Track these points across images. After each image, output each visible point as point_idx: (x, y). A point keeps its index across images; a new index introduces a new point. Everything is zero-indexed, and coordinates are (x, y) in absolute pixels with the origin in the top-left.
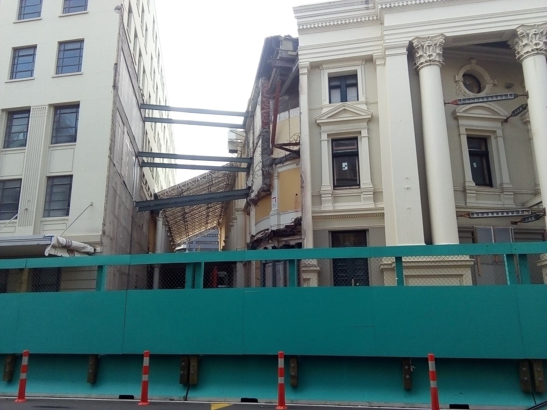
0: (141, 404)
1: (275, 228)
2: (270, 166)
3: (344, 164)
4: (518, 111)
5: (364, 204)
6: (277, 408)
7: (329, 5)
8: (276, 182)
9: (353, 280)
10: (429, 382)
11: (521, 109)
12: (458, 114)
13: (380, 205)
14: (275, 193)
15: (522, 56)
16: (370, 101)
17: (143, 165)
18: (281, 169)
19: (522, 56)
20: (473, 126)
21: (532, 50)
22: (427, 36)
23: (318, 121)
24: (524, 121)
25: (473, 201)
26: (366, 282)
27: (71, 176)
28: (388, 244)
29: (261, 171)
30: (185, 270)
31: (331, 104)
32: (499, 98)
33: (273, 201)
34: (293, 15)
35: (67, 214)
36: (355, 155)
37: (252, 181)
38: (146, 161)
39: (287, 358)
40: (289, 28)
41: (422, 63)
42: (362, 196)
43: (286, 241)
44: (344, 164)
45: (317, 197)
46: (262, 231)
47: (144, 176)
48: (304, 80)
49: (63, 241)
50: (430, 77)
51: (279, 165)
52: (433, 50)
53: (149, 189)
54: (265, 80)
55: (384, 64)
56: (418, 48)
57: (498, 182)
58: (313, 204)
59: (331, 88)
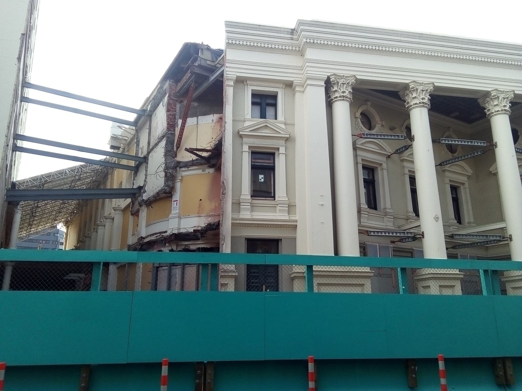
1: (176, 232)
3: (261, 176)
4: (401, 150)
5: (278, 215)
7: (259, 27)
8: (178, 185)
9: (264, 286)
10: (440, 380)
11: (404, 149)
12: (357, 146)
13: (293, 218)
14: (177, 196)
16: (288, 122)
18: (185, 173)
19: (411, 106)
20: (367, 157)
21: (420, 103)
22: (342, 75)
23: (241, 133)
24: (402, 158)
25: (366, 221)
26: (276, 288)
30: (92, 270)
33: (174, 204)
34: (223, 29)
36: (272, 169)
39: (447, 361)
40: (217, 41)
41: (336, 97)
42: (278, 208)
43: (186, 245)
44: (261, 176)
45: (237, 205)
46: (156, 234)
50: (342, 110)
51: (184, 169)
54: (173, 82)
55: (303, 92)
56: (334, 84)
57: (382, 206)
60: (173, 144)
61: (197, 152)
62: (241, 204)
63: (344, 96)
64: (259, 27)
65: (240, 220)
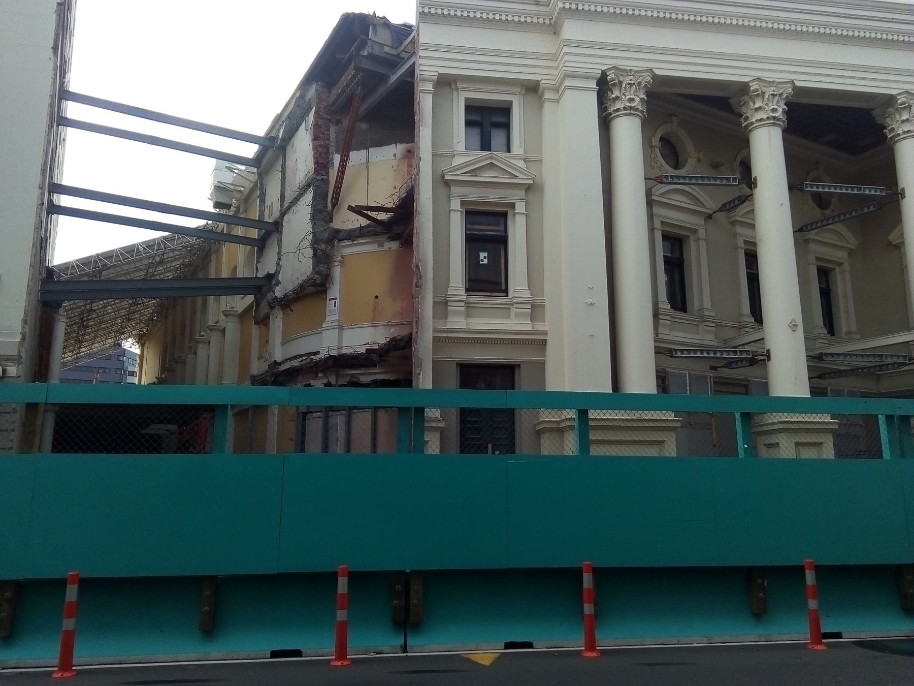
0: (59, 675)
1: (334, 353)
3: (483, 255)
4: (732, 205)
5: (515, 323)
6: (333, 663)
8: (337, 271)
9: (490, 446)
13: (540, 328)
14: (335, 291)
15: (610, 114)
16: (531, 156)
18: (348, 250)
21: (768, 118)
22: (629, 68)
23: (447, 177)
24: (733, 219)
25: (667, 332)
26: (509, 446)
28: (549, 388)
32: (718, 182)
33: (330, 305)
39: (820, 570)
41: (618, 110)
43: (353, 376)
44: (483, 255)
45: (442, 305)
46: (300, 356)
50: (628, 133)
51: (345, 243)
52: (778, 102)
55: (558, 101)
56: (614, 85)
58: (435, 316)
62: (449, 304)
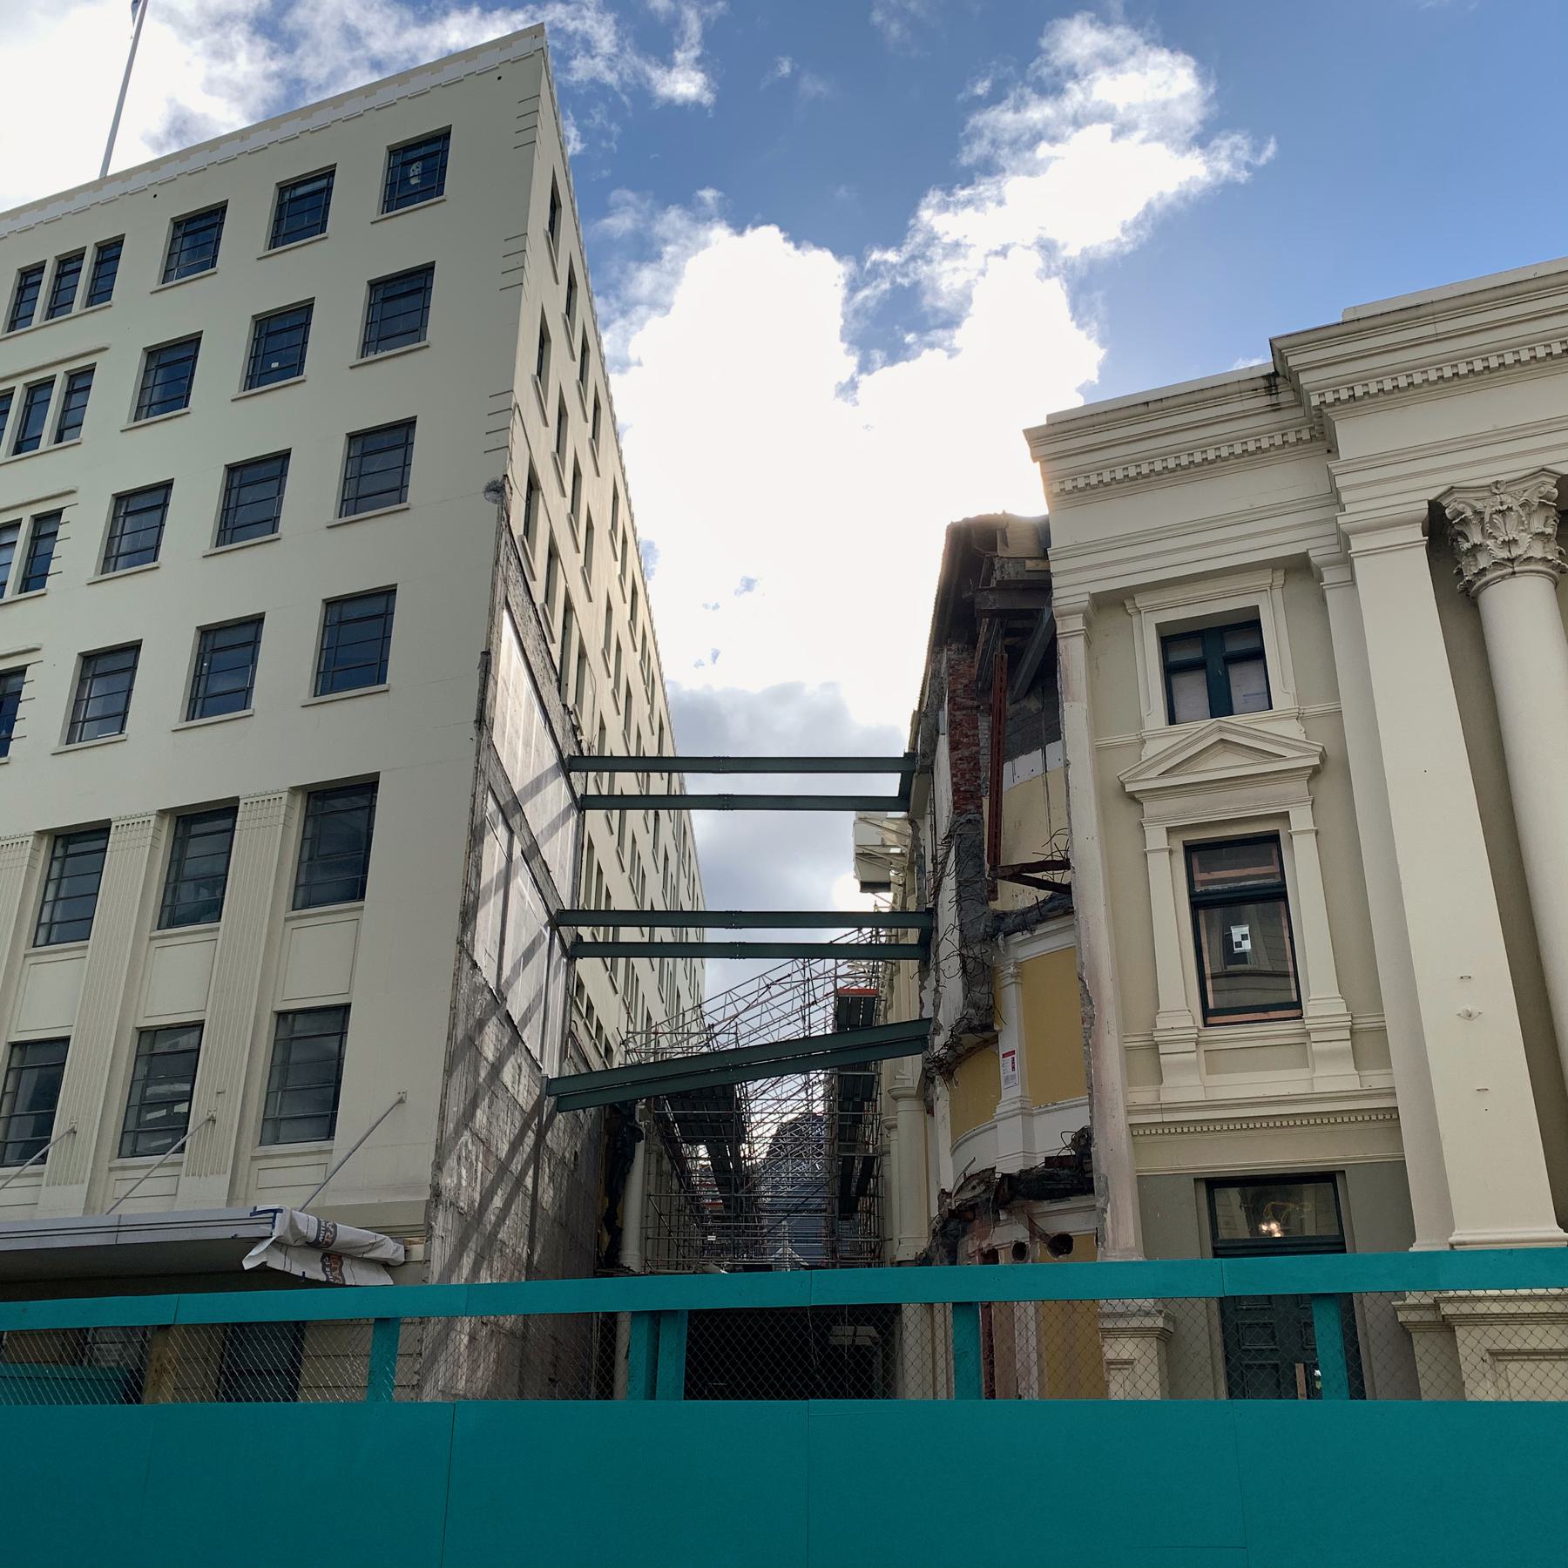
1: (1013, 1167)
2: (990, 933)
3: (1237, 932)
5: (1333, 1077)
8: (1012, 1000)
14: (1011, 1038)
17: (576, 950)
23: (1129, 788)
27: (347, 1008)
29: (958, 959)
31: (1174, 728)
35: (330, 1134)
36: (1276, 895)
37: (936, 991)
38: (587, 938)
40: (1019, 494)
44: (1237, 932)
47: (580, 986)
48: (1073, 655)
49: (309, 1226)
51: (1018, 937)
53: (599, 1027)
58: (1130, 1080)
59: (1171, 670)
60: (979, 857)
61: (1038, 875)
62: (1162, 1049)
63: (1512, 560)
64: (1144, 408)
65: (1162, 1111)
